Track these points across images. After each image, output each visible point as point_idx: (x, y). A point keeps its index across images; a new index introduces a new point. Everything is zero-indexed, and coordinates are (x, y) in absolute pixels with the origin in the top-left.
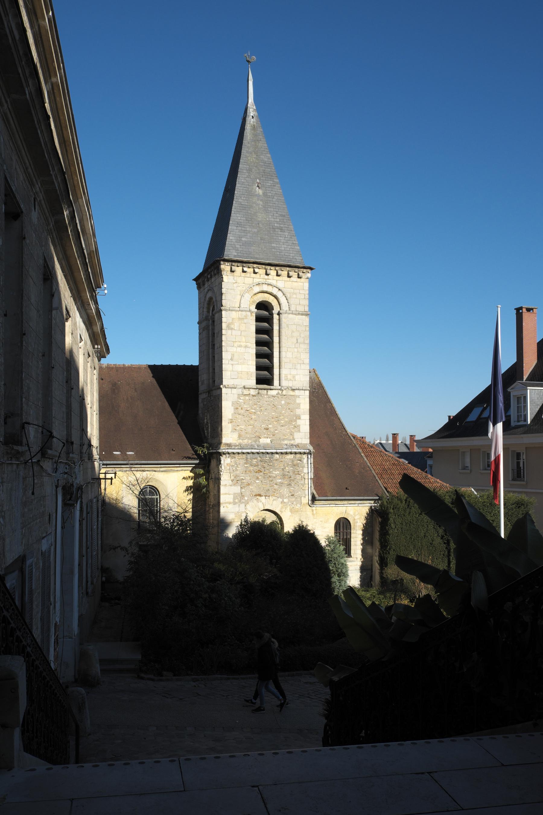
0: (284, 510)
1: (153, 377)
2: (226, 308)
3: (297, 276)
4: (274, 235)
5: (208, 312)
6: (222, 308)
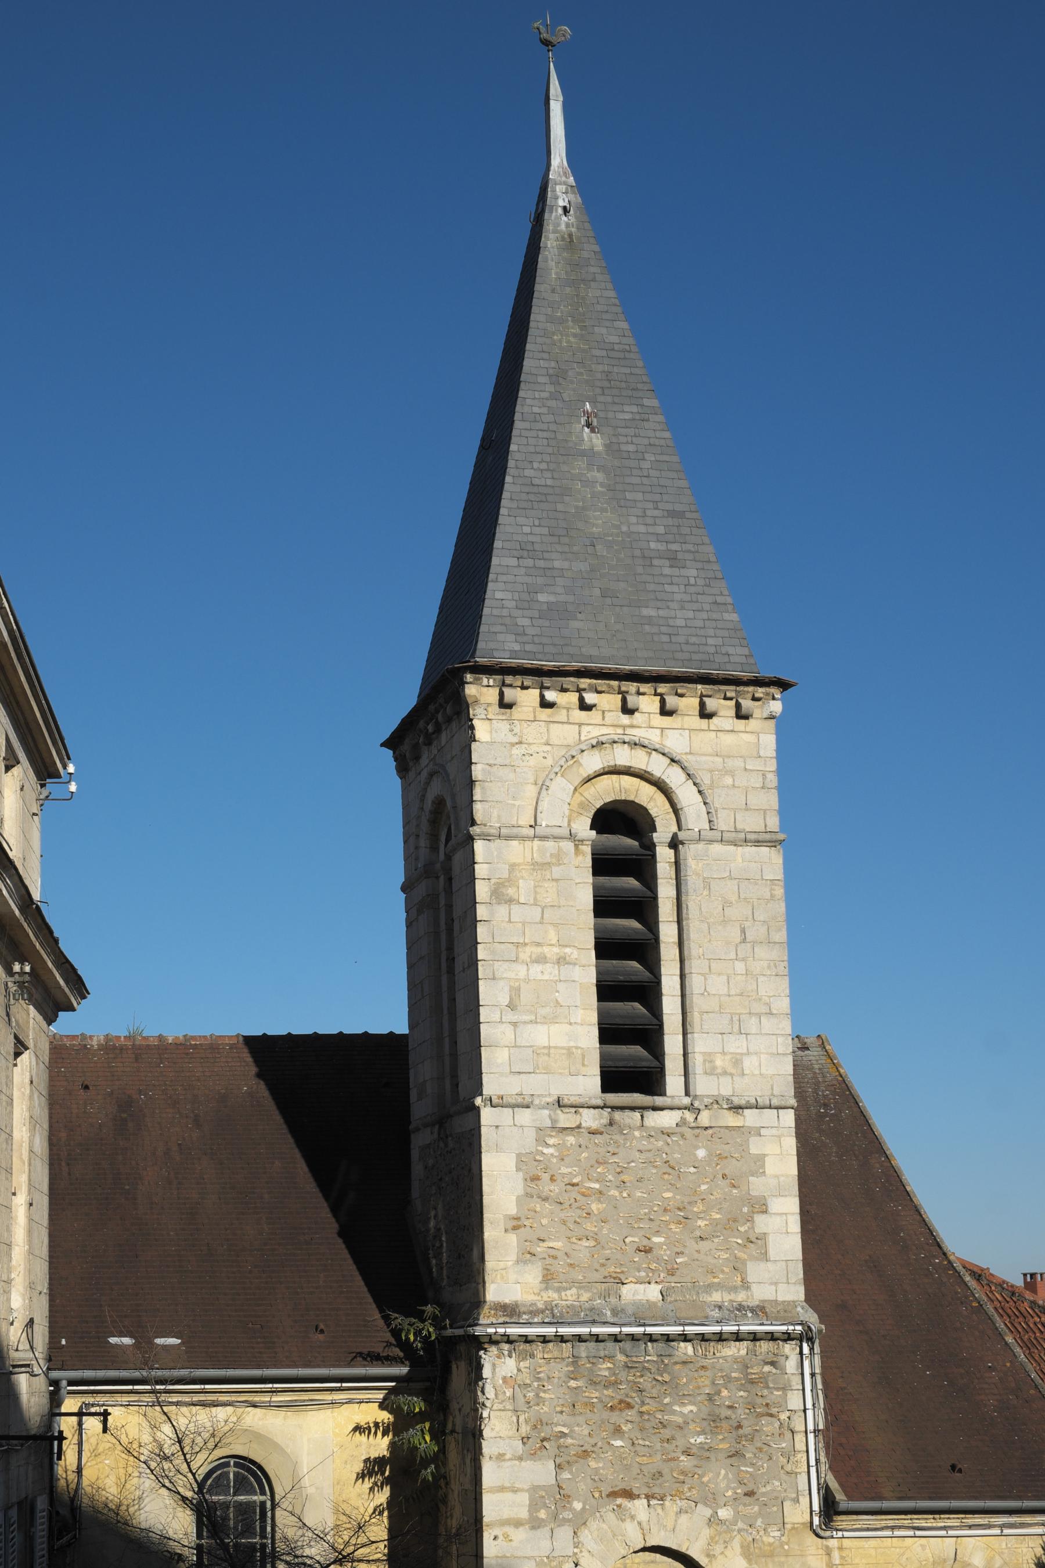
0: (718, 1549)
1: (259, 1075)
2: (485, 830)
3: (733, 713)
4: (649, 578)
5: (434, 848)
6: (474, 830)
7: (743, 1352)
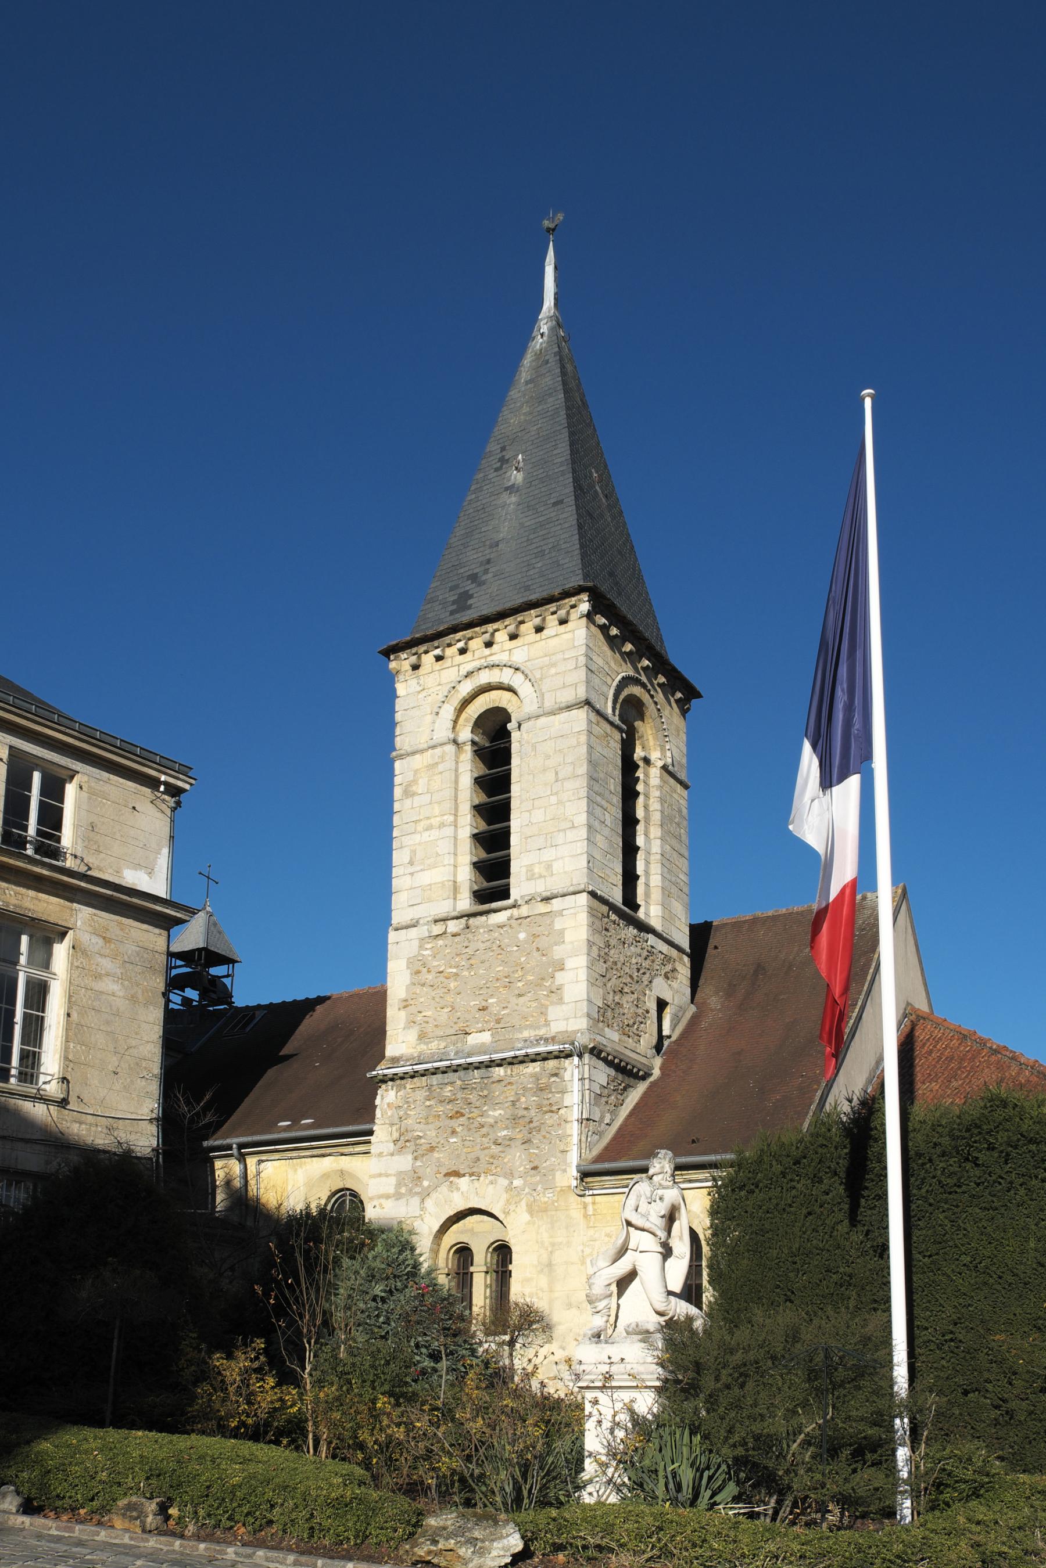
0: (512, 1207)
7: (538, 1069)
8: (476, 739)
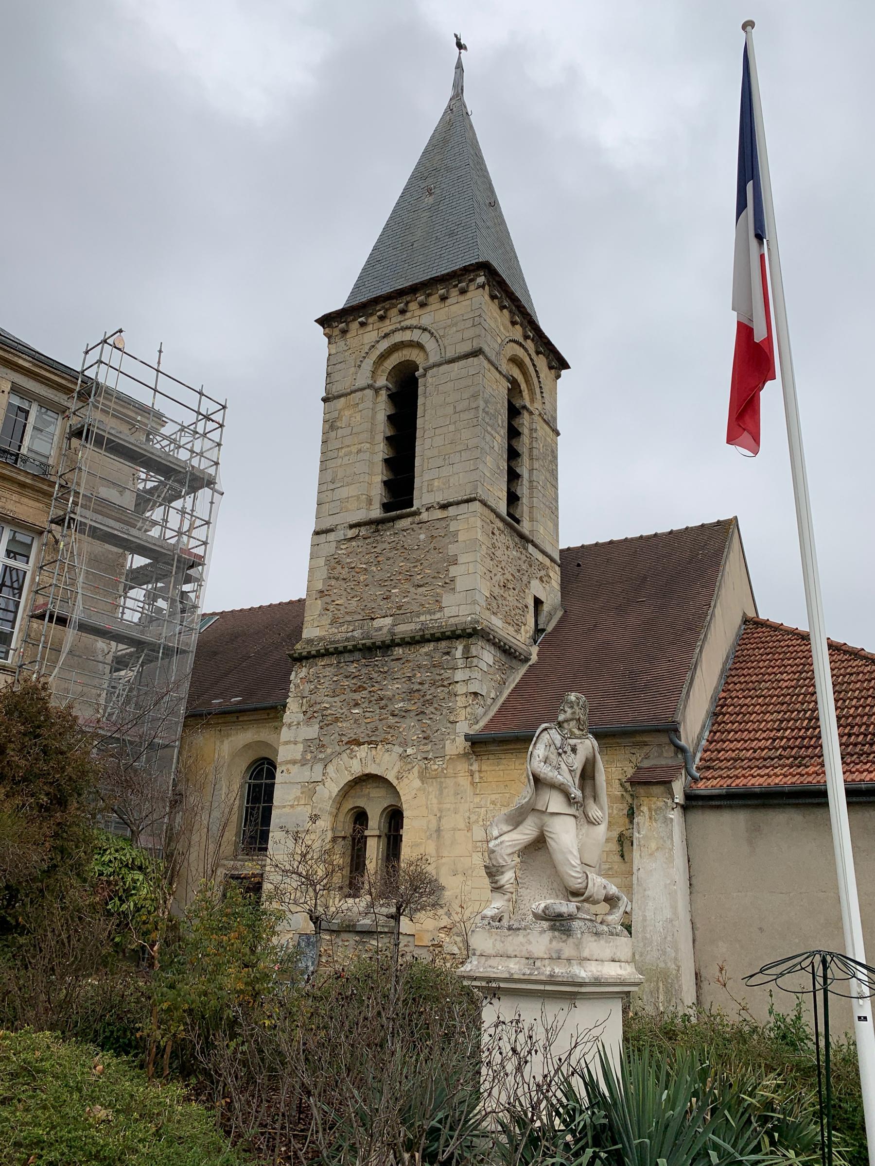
8: (390, 386)
